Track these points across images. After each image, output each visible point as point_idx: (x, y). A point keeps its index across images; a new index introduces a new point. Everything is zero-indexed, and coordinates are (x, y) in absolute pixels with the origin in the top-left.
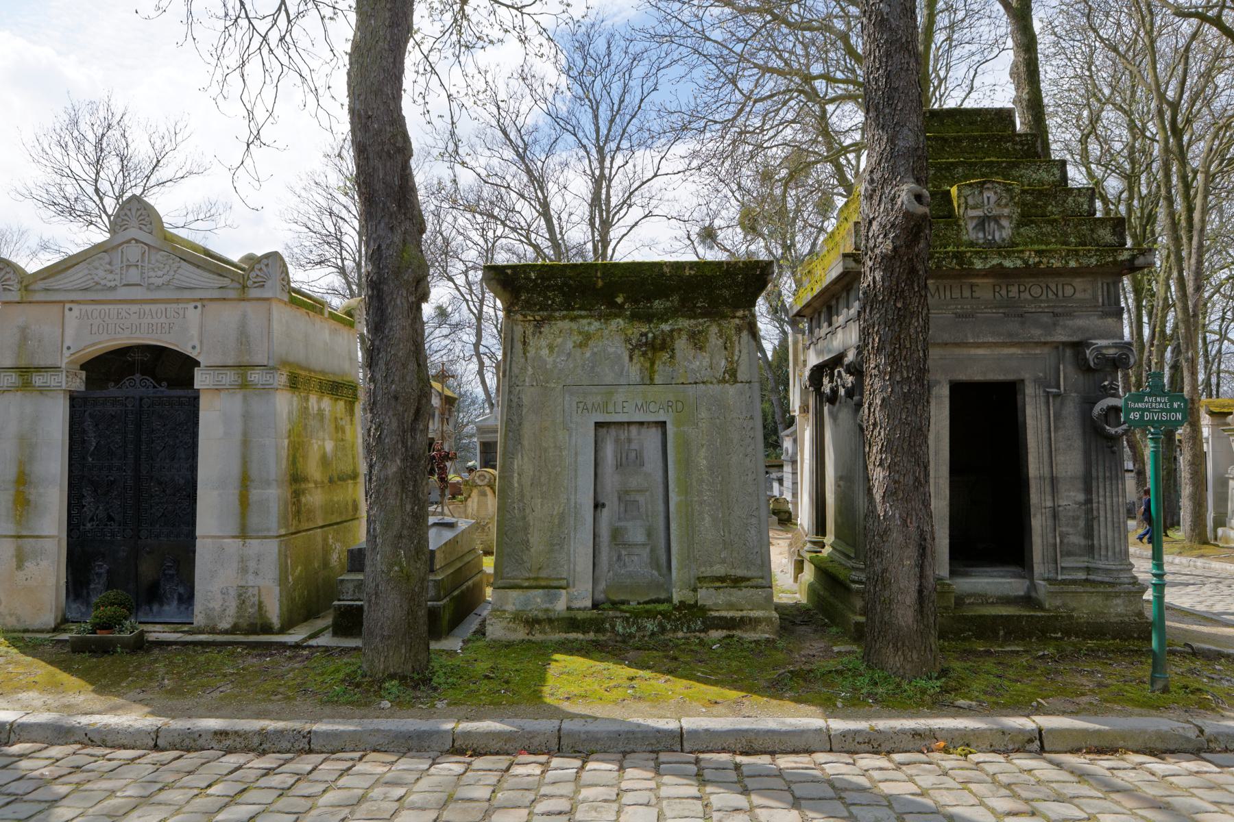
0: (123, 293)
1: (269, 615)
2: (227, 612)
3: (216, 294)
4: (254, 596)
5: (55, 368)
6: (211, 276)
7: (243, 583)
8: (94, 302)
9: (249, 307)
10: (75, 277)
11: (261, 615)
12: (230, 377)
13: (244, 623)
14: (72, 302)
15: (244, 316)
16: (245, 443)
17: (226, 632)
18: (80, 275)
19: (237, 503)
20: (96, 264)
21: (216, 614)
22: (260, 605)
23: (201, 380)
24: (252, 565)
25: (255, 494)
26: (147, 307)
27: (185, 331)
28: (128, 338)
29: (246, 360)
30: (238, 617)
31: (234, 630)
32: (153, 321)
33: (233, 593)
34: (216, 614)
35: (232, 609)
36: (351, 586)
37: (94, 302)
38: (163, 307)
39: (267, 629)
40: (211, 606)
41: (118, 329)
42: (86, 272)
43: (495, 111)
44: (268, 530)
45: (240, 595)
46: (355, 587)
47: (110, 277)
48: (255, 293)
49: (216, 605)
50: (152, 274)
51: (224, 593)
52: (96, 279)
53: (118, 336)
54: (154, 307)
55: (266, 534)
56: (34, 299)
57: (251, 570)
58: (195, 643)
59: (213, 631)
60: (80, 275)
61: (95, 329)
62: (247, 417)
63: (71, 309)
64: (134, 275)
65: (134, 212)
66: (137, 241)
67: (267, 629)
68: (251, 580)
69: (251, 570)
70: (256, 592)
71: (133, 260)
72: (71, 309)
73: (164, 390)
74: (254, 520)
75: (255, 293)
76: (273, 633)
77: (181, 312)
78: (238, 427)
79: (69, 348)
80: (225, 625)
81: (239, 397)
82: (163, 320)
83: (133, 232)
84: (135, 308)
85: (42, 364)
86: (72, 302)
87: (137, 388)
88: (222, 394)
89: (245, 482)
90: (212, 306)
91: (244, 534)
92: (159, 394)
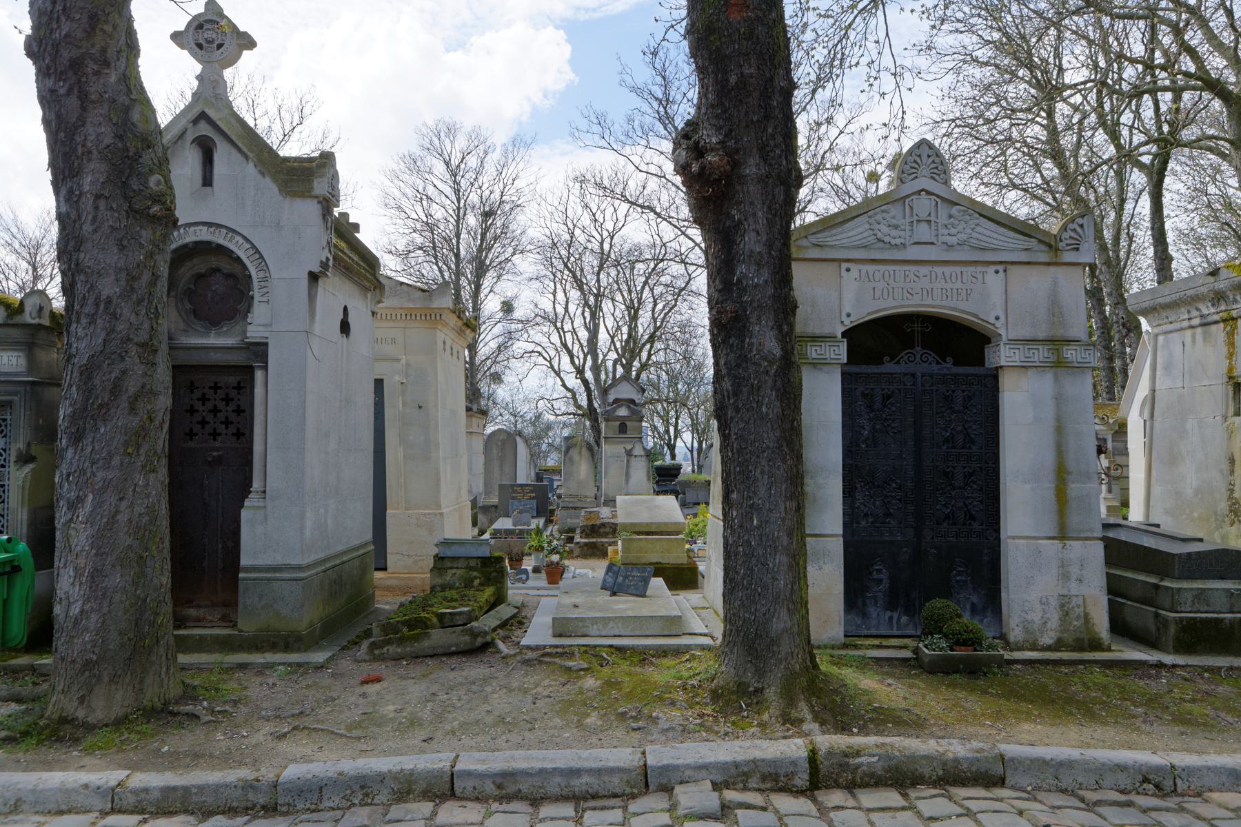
0: (913, 253)
1: (1097, 629)
2: (1049, 625)
3: (1023, 257)
4: (1078, 606)
5: (830, 338)
6: (1011, 234)
7: (1065, 592)
8: (874, 261)
9: (1059, 272)
10: (854, 233)
11: (1088, 629)
12: (1041, 354)
13: (1069, 638)
14: (848, 260)
15: (1055, 283)
16: (1060, 429)
17: (1049, 648)
18: (860, 229)
19: (1053, 499)
20: (879, 217)
21: (1036, 627)
22: (1086, 616)
23: (1003, 355)
24: (1074, 571)
25: (1074, 489)
26: (939, 270)
27: (982, 298)
28: (916, 306)
29: (1060, 333)
30: (1062, 631)
31: (1058, 646)
32: (948, 286)
33: (1054, 602)
34: (1036, 627)
35: (1054, 623)
36: (1189, 596)
37: (874, 261)
38: (958, 269)
39: (1096, 645)
40: (1029, 618)
41: (906, 294)
42: (867, 226)
43: (296, 121)
44: (1091, 530)
45: (1062, 606)
46: (1195, 597)
47: (894, 233)
48: (1069, 257)
49: (1036, 617)
50: (946, 232)
51: (1044, 603)
52: (880, 235)
53: (907, 302)
54: (947, 270)
55: (1089, 534)
56: (807, 256)
57: (1074, 577)
58: (1082, 662)
59: (1034, 648)
60: (860, 229)
61: (878, 293)
62: (1059, 399)
63: (848, 270)
64: (924, 233)
65: (924, 158)
66: (929, 193)
67: (1096, 645)
68: (1074, 588)
69: (1074, 577)
70: (1081, 602)
71: (924, 216)
72: (848, 270)
73: (949, 367)
74: (1074, 520)
75: (1069, 257)
76: (1103, 650)
77: (980, 276)
78: (1049, 412)
79: (849, 315)
80: (1047, 640)
81: (1049, 377)
82: (959, 285)
83: (924, 183)
84: (924, 270)
85: (817, 332)
86: (848, 260)
87: (918, 364)
88: (1030, 372)
89: (1062, 475)
90: (1013, 270)
91: (1063, 535)
92: (945, 371)
